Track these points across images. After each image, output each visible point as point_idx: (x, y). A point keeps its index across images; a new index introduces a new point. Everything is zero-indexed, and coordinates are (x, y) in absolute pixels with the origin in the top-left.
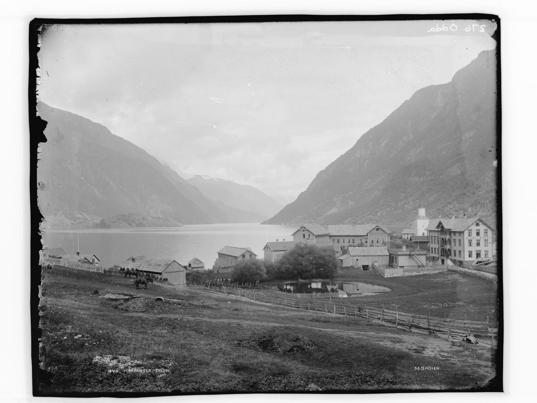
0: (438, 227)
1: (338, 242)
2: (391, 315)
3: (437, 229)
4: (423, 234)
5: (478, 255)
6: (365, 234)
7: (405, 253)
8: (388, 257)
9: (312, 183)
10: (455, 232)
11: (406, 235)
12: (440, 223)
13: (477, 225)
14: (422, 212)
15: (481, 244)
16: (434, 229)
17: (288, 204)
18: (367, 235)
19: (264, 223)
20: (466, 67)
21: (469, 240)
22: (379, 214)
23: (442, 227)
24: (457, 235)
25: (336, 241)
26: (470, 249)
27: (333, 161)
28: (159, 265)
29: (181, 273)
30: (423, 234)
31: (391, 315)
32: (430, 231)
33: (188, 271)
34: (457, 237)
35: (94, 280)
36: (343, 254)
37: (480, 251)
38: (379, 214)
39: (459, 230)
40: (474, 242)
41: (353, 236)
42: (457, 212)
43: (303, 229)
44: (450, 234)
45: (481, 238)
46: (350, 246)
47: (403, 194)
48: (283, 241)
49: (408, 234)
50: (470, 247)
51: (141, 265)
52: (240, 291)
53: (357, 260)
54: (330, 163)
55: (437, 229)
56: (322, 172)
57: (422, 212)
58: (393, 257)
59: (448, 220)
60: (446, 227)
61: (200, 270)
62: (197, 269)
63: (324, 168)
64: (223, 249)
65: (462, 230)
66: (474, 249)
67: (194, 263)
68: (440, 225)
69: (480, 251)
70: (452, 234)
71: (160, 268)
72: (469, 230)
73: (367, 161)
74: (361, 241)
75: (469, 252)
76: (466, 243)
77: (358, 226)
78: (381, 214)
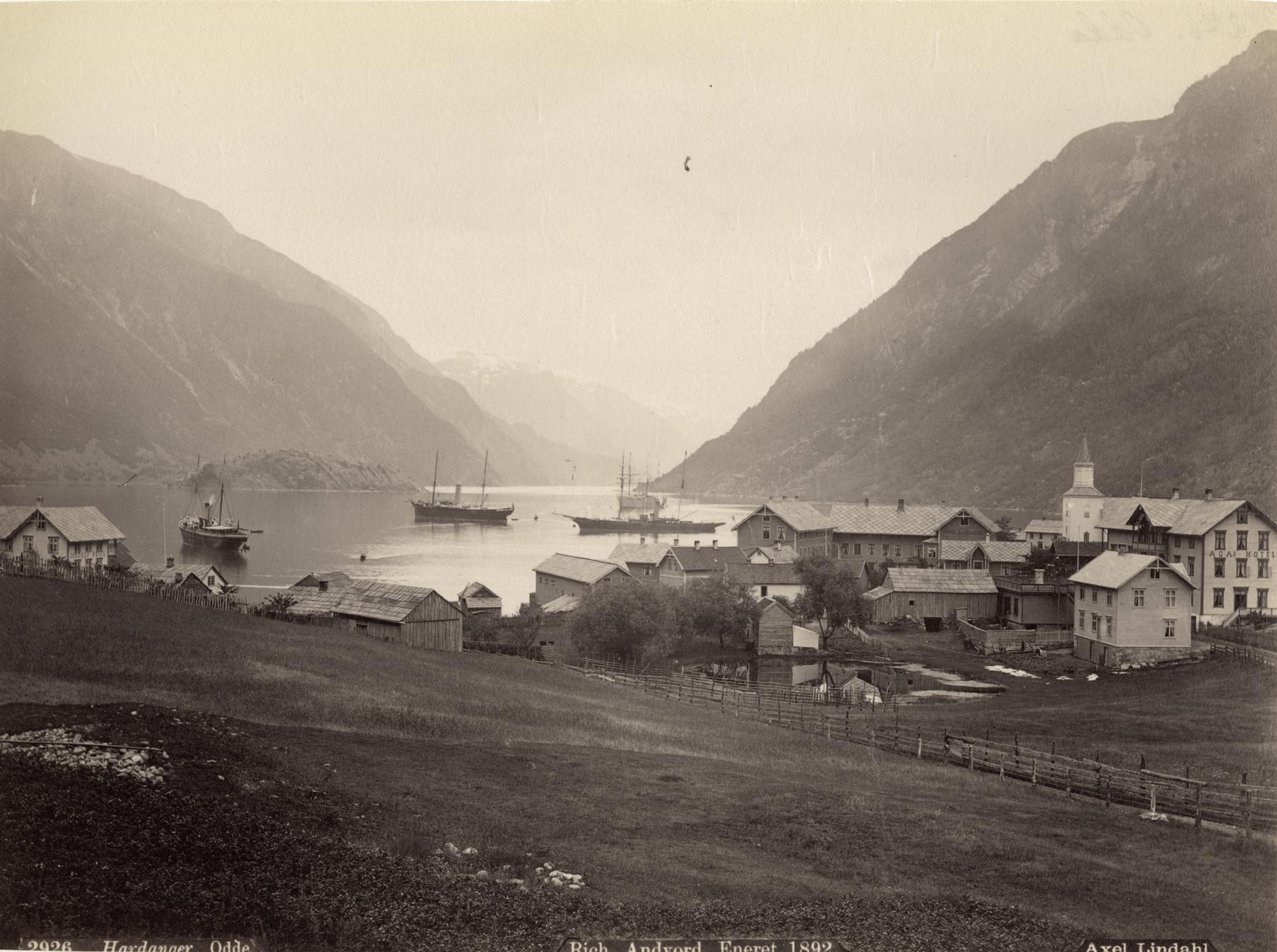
0: (1132, 521)
1: (858, 551)
3: (1130, 528)
4: (1086, 535)
5: (1240, 600)
7: (1042, 590)
8: (995, 599)
10: (1179, 538)
13: (1242, 520)
15: (934, 636)
16: (1122, 525)
18: (936, 537)
20: (1214, 75)
21: (1216, 560)
23: (1145, 522)
24: (1185, 544)
25: (851, 549)
26: (1219, 583)
28: (394, 602)
29: (451, 627)
30: (1086, 535)
32: (1111, 531)
34: (1184, 551)
37: (1246, 589)
39: (1190, 533)
40: (1230, 567)
42: (1176, 476)
44: (1166, 542)
45: (1249, 554)
48: (1082, 539)
49: (1041, 535)
50: (1219, 579)
53: (912, 603)
55: (1130, 528)
57: (1085, 476)
58: (1008, 599)
60: (1156, 521)
63: (812, 345)
64: (542, 564)
65: (1200, 532)
66: (1230, 582)
67: (474, 596)
68: (1139, 516)
69: (1246, 589)
70: (1172, 543)
72: (1217, 533)
74: (917, 549)
75: (1216, 590)
76: (1210, 565)
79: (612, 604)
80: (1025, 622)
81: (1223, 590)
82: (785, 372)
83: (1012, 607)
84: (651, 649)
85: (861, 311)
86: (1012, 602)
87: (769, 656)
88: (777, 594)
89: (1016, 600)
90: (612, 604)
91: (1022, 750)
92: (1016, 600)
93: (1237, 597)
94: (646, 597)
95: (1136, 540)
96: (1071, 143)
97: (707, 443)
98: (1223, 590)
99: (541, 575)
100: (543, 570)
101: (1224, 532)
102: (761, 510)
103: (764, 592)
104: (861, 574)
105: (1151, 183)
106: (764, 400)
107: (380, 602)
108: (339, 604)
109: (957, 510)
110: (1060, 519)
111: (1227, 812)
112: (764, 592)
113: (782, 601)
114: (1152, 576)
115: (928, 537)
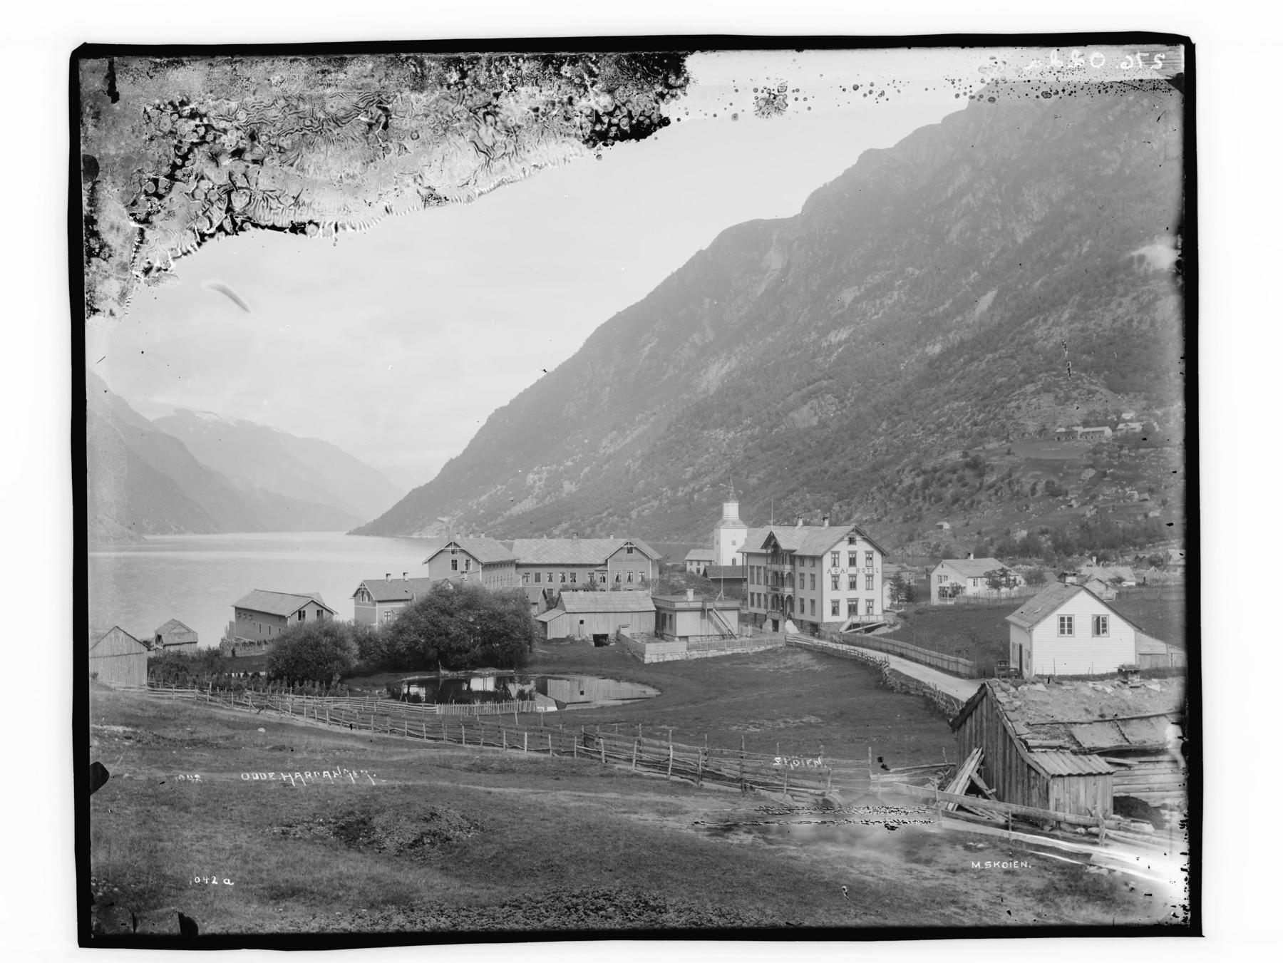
0: (765, 546)
3: (764, 551)
4: (734, 560)
5: (853, 609)
10: (802, 558)
11: (695, 564)
14: (731, 510)
16: (758, 549)
19: (359, 532)
20: (831, 183)
21: (833, 576)
23: (776, 546)
24: (808, 563)
26: (836, 595)
30: (734, 560)
32: (750, 555)
36: (549, 608)
37: (856, 600)
39: (811, 554)
40: (844, 581)
41: (573, 566)
46: (565, 589)
48: (730, 564)
49: (699, 561)
50: (836, 592)
52: (291, 700)
55: (764, 551)
56: (500, 412)
57: (731, 510)
58: (665, 615)
62: (177, 648)
63: (506, 403)
66: (844, 595)
68: (771, 541)
69: (856, 600)
70: (797, 562)
81: (872, 601)
93: (850, 607)
96: (720, 235)
98: (872, 601)
99: (240, 611)
100: (239, 606)
101: (838, 553)
105: (785, 270)
106: (465, 451)
109: (624, 541)
110: (712, 548)
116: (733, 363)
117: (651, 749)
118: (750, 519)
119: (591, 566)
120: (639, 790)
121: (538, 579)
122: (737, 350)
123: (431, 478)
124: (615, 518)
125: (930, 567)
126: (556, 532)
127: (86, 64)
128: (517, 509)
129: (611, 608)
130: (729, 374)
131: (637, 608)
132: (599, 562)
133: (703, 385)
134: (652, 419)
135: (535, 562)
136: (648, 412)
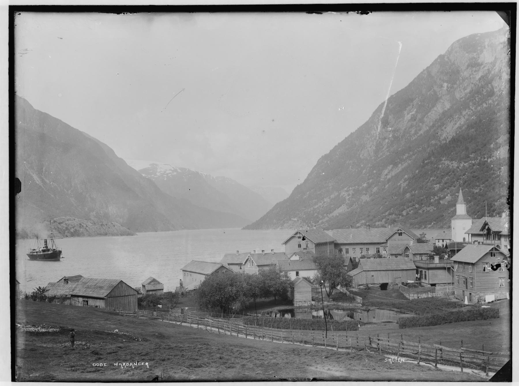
0: (483, 229)
2: (412, 348)
4: (464, 239)
6: (384, 241)
7: (439, 265)
9: (312, 172)
11: (441, 241)
12: (486, 224)
14: (461, 209)
17: (278, 202)
19: (248, 228)
22: (404, 213)
23: (489, 230)
27: (340, 141)
28: (101, 288)
30: (464, 239)
31: (412, 348)
32: (473, 235)
33: (140, 296)
35: (257, 291)
36: (353, 269)
38: (404, 213)
41: (367, 244)
43: (298, 235)
46: (363, 257)
47: (438, 185)
51: (76, 287)
52: (210, 320)
53: (373, 276)
54: (336, 144)
55: (481, 233)
56: (325, 157)
57: (461, 209)
58: (421, 272)
59: (496, 219)
60: (494, 229)
61: (159, 293)
62: (154, 293)
63: (328, 152)
67: (149, 284)
71: (103, 291)
73: (387, 141)
77: (374, 231)
78: (408, 214)
79: (217, 284)
80: (431, 283)
82: (315, 167)
83: (424, 275)
84: (236, 306)
85: (352, 133)
86: (424, 273)
87: (300, 307)
88: (306, 276)
89: (425, 272)
90: (217, 284)
91: (405, 342)
92: (425, 272)
94: (233, 280)
95: (485, 239)
97: (277, 204)
102: (297, 233)
103: (297, 274)
104: (347, 263)
107: (94, 288)
108: (73, 290)
111: (278, 338)
112: (297, 274)
113: (307, 279)
114: (492, 256)
115: (383, 243)
116: (462, 121)
117: (409, 347)
118: (474, 213)
119: (378, 243)
120: (481, 369)
121: (347, 252)
122: (464, 113)
123: (286, 197)
124: (394, 216)
125: (133, 301)
126: (358, 225)
127: (21, 18)
128: (336, 213)
129: (389, 268)
130: (460, 128)
131: (405, 267)
132: (382, 241)
133: (444, 135)
134: (414, 157)
135: (345, 242)
136: (411, 153)
